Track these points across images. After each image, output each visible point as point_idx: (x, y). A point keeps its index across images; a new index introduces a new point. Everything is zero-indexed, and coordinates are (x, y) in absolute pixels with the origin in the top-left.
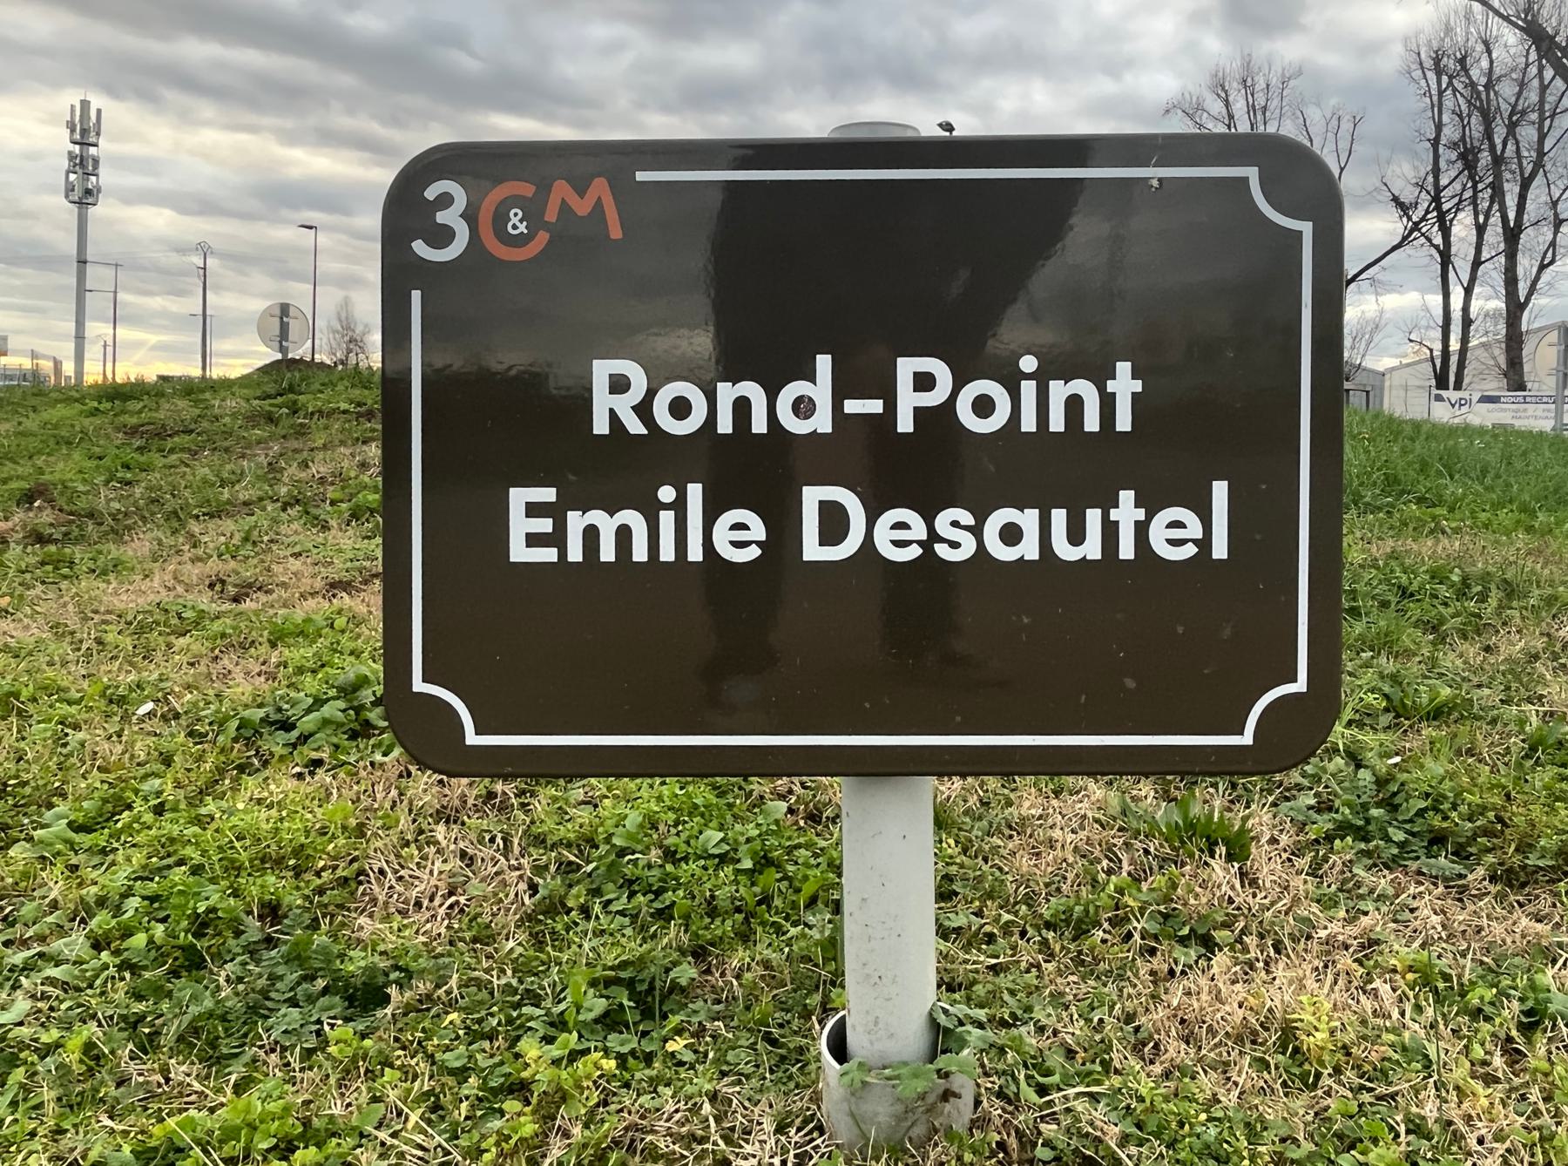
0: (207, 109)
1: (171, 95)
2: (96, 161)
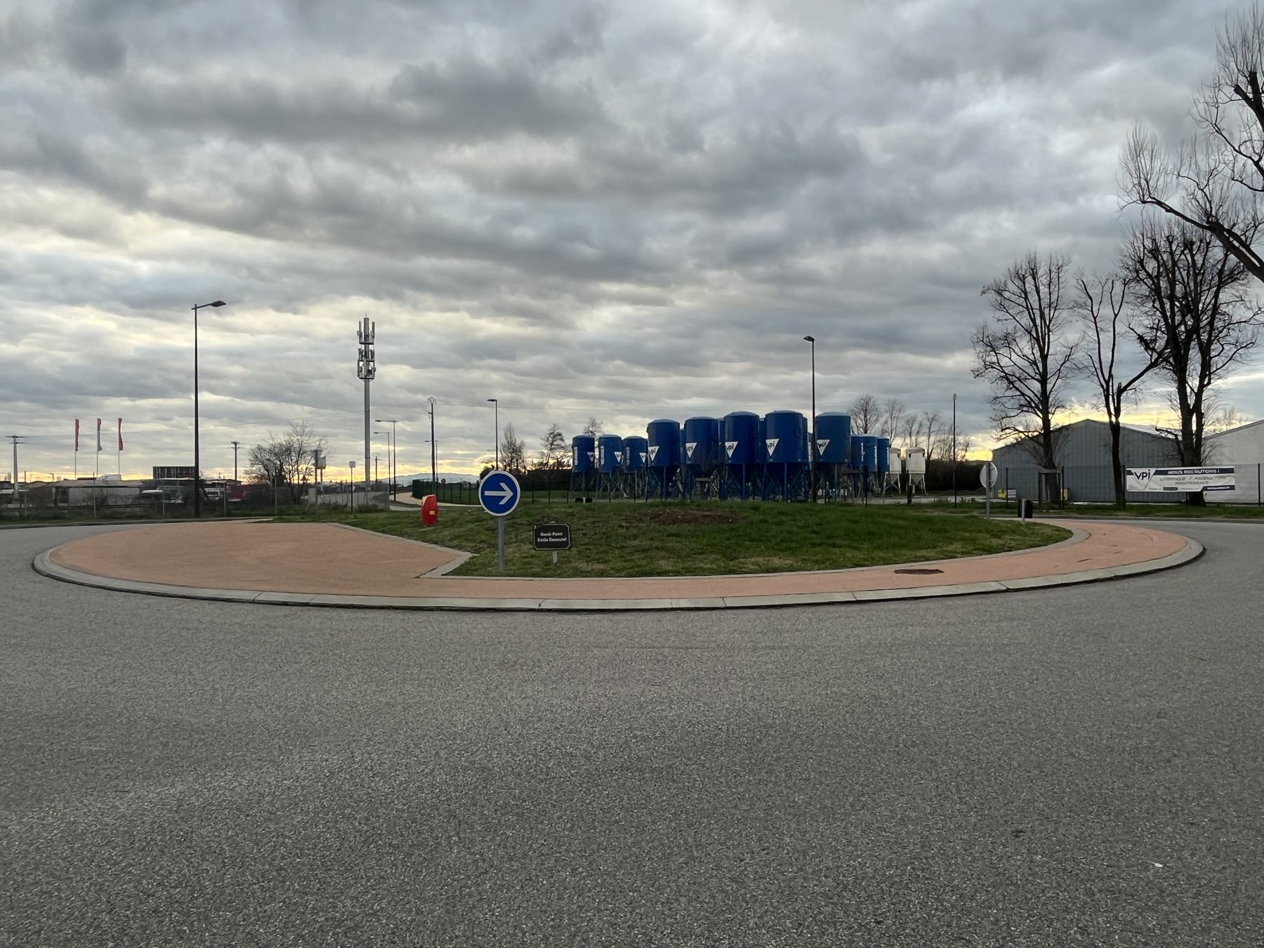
0: (428, 299)
1: (409, 293)
2: (373, 353)
